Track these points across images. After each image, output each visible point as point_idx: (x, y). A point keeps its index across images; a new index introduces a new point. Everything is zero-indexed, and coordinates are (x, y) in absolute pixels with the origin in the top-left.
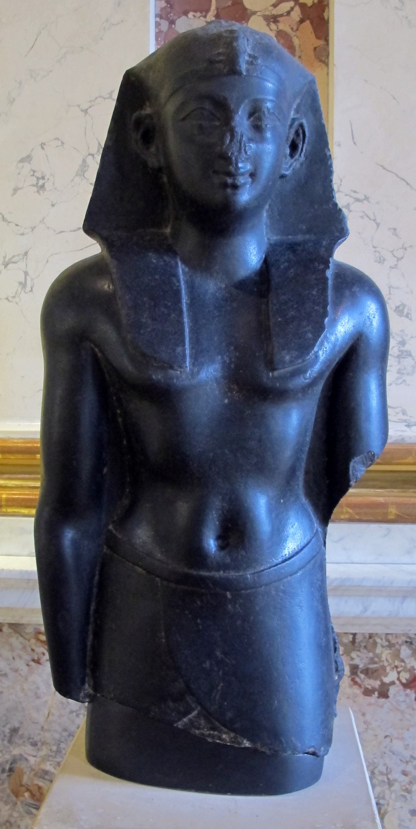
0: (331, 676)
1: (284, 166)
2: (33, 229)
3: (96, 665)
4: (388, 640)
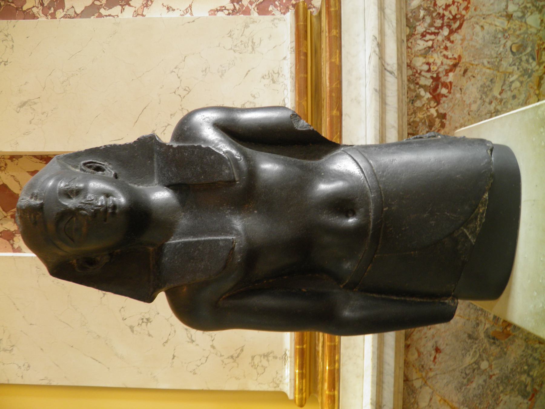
0: (439, 140)
1: (109, 175)
2: (172, 325)
3: (433, 296)
4: (412, 114)
